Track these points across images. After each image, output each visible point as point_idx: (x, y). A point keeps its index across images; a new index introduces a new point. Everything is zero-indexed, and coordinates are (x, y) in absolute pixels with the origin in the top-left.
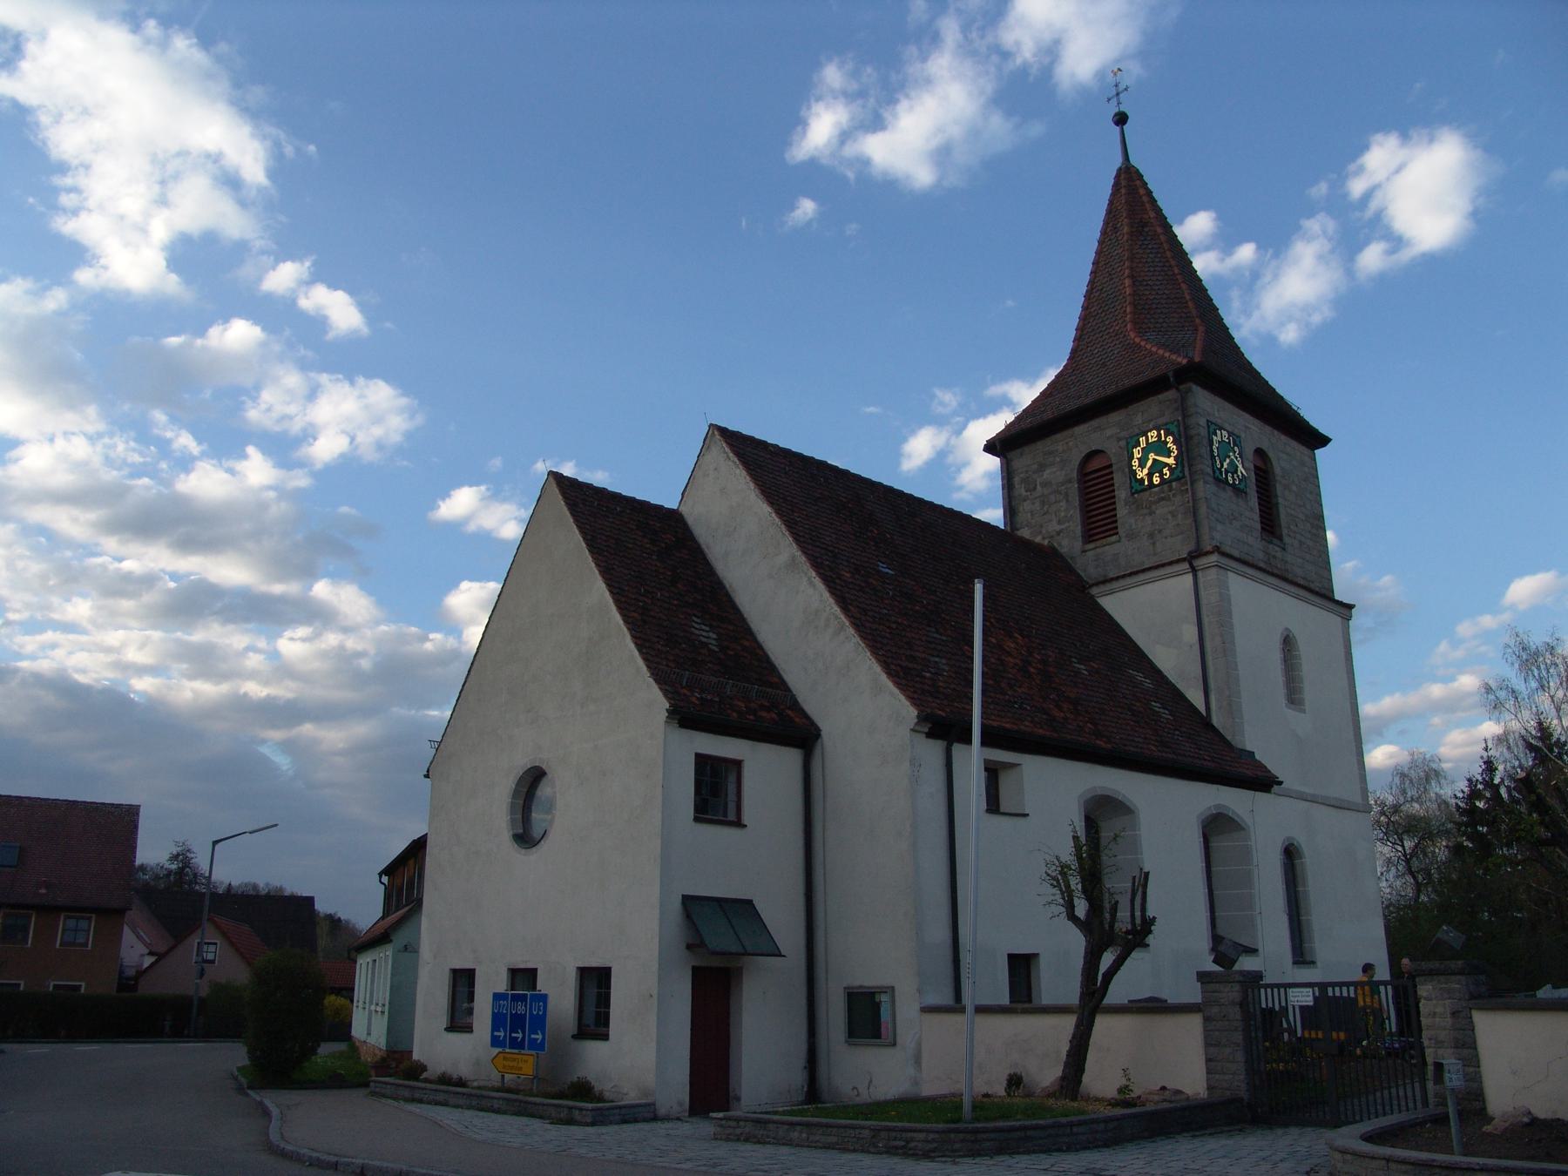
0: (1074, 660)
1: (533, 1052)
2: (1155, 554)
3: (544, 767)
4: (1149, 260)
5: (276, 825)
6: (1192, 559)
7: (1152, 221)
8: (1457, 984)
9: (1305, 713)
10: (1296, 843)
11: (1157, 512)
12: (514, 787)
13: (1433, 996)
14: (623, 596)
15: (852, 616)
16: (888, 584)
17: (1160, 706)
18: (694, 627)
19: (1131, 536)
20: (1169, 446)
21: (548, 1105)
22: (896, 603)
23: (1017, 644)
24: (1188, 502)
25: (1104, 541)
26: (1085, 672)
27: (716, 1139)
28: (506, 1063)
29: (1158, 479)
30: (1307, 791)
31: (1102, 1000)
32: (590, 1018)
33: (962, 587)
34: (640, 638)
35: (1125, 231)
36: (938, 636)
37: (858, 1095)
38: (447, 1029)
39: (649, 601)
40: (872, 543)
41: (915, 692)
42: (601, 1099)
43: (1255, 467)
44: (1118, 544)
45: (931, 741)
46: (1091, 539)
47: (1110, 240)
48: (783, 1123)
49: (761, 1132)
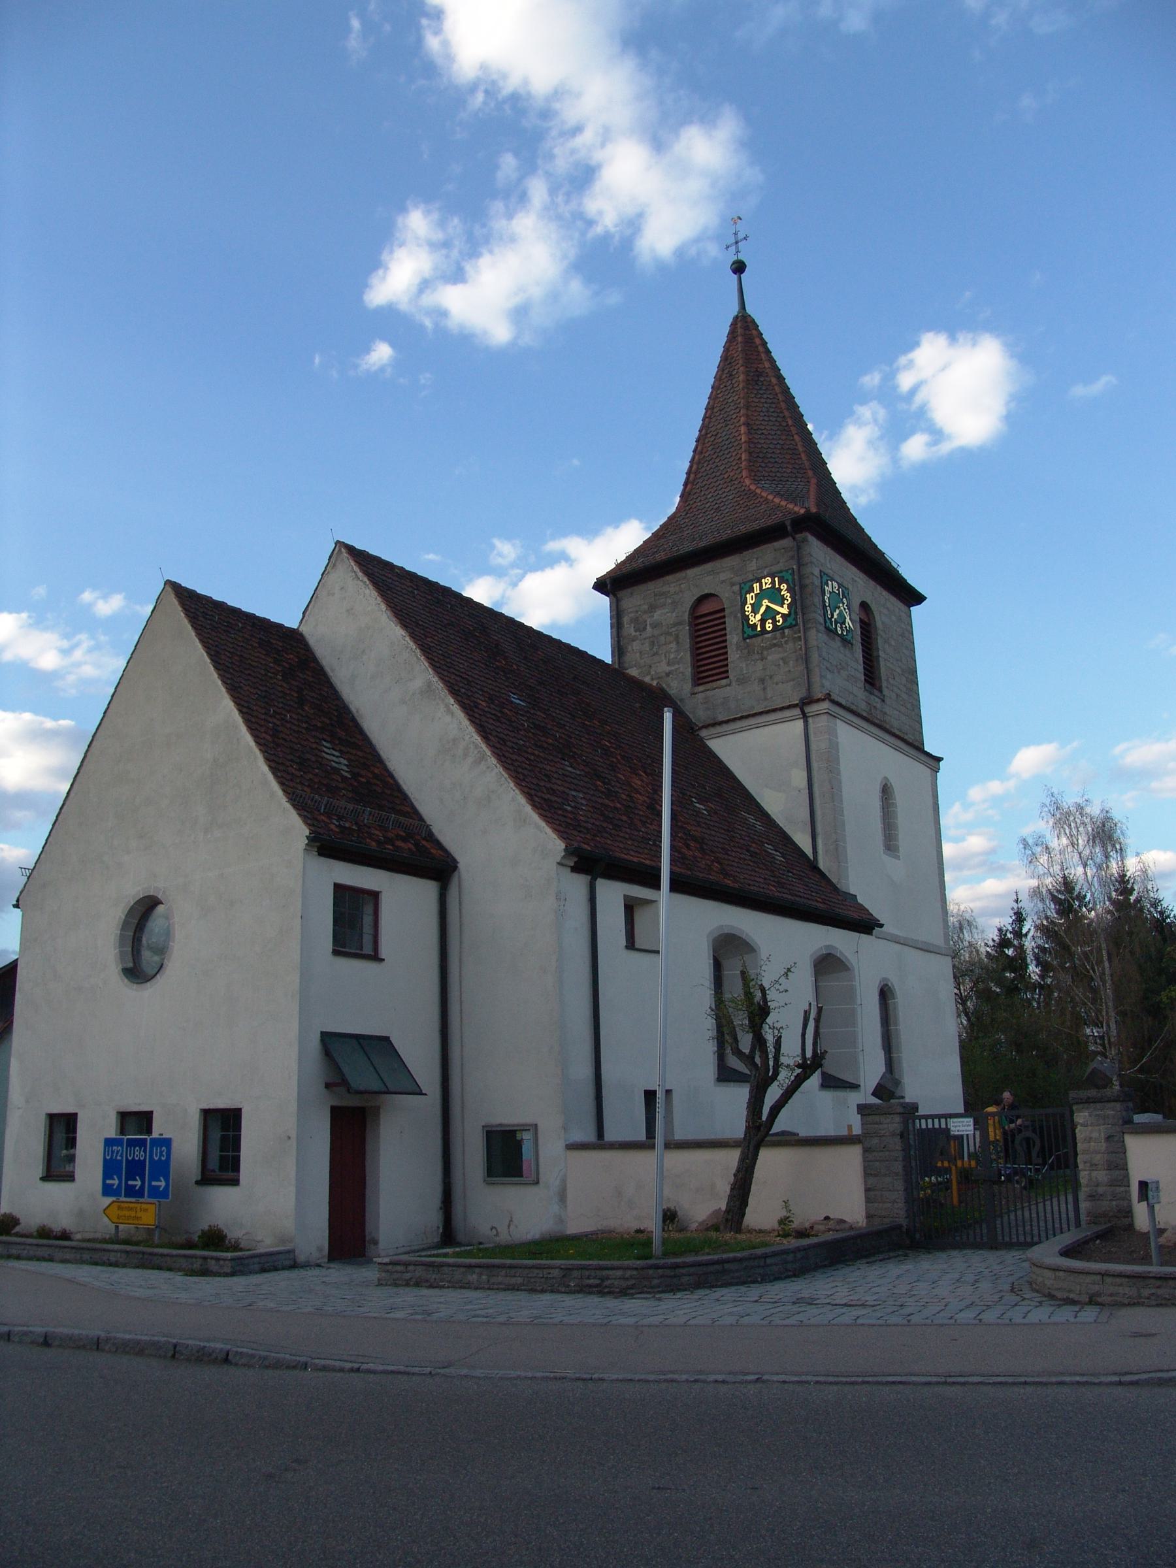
0: (694, 800)
2: (766, 699)
4: (764, 410)
7: (767, 371)
8: (1112, 1111)
11: (769, 658)
12: (124, 917)
15: (494, 746)
17: (772, 848)
18: (324, 752)
19: (742, 681)
20: (782, 593)
25: (714, 685)
29: (771, 625)
32: (214, 1163)
36: (573, 771)
37: (497, 1235)
38: (43, 1179)
41: (560, 825)
42: (236, 1247)
44: (728, 687)
45: (575, 875)
48: (459, 1266)
49: (434, 1277)
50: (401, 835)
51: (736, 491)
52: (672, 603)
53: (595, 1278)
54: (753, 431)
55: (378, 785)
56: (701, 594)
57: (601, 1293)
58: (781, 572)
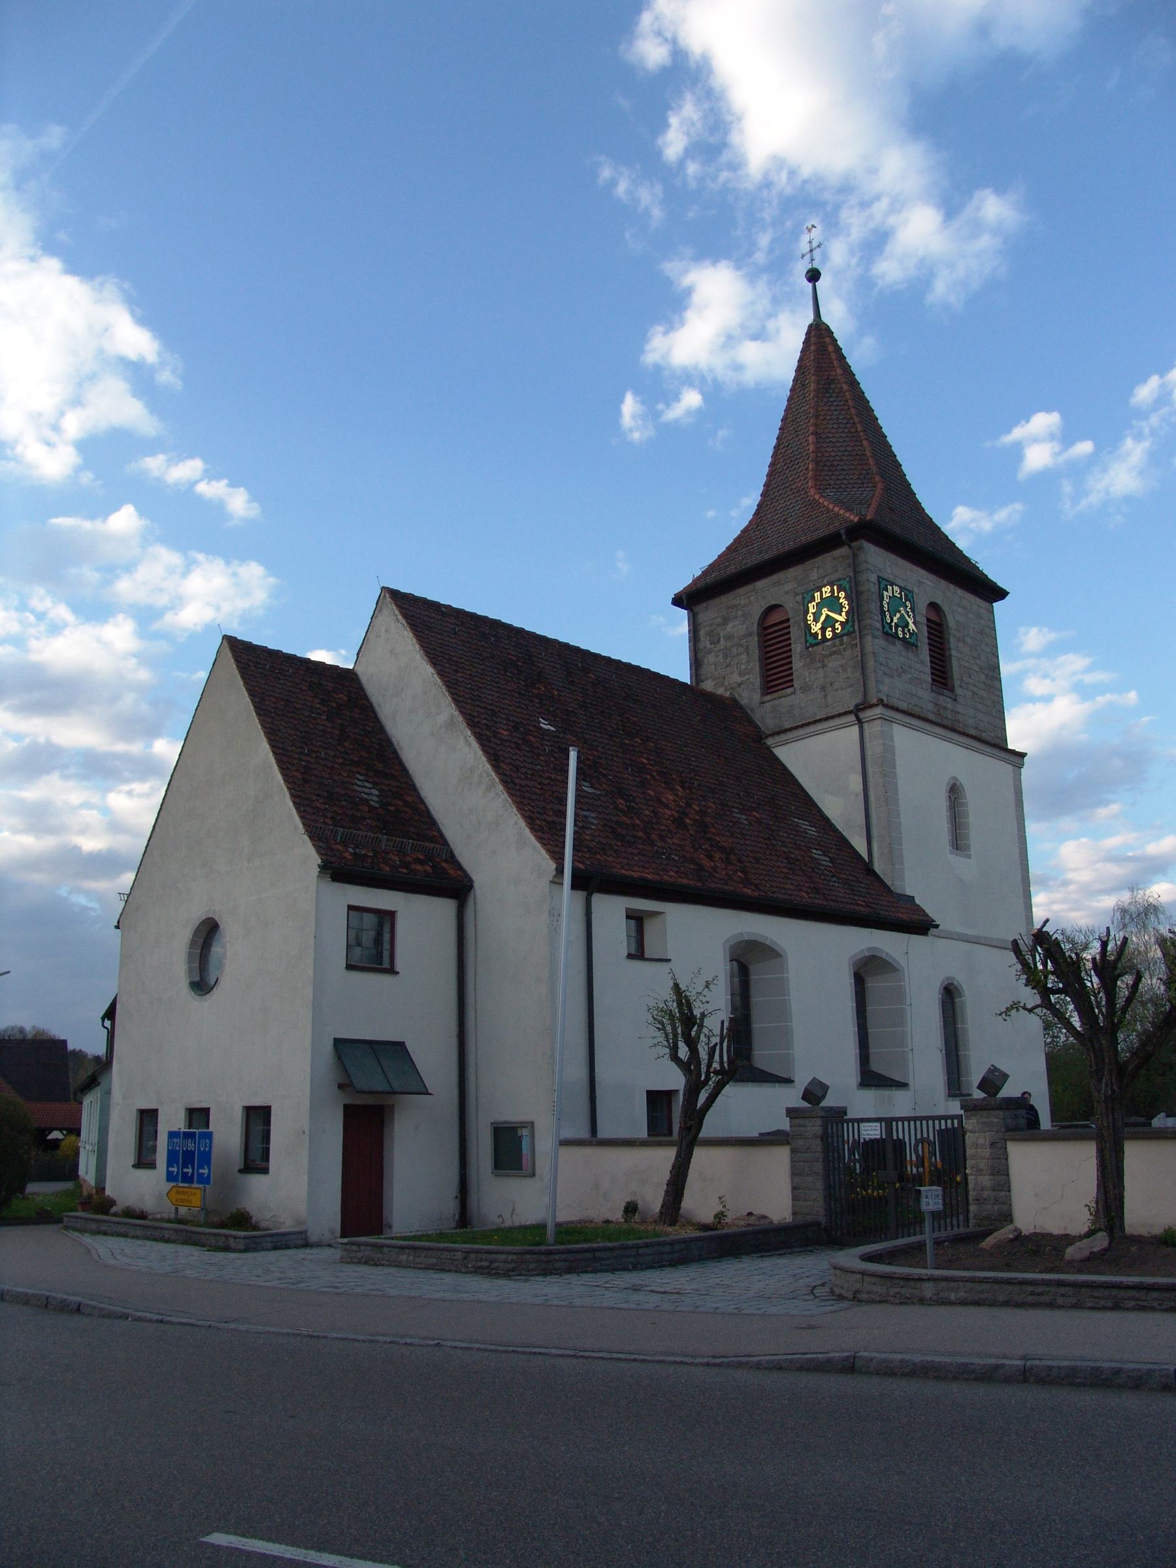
0: (736, 810)
1: (201, 1186)
2: (827, 706)
3: (216, 919)
5: (8, 972)
6: (857, 711)
11: (830, 665)
12: (191, 937)
13: (977, 1129)
16: (547, 740)
17: (820, 853)
19: (806, 688)
20: (841, 601)
23: (677, 795)
25: (779, 694)
26: (746, 822)
27: (342, 1262)
29: (831, 633)
31: (698, 1134)
32: (256, 1154)
33: (627, 741)
34: (299, 797)
35: (812, 387)
37: (503, 1222)
40: (537, 701)
42: (255, 1227)
43: (928, 620)
46: (769, 691)
48: (393, 1247)
50: (419, 859)
53: (486, 1260)
54: (821, 441)
55: (405, 812)
56: (768, 605)
57: (489, 1274)
58: (839, 580)
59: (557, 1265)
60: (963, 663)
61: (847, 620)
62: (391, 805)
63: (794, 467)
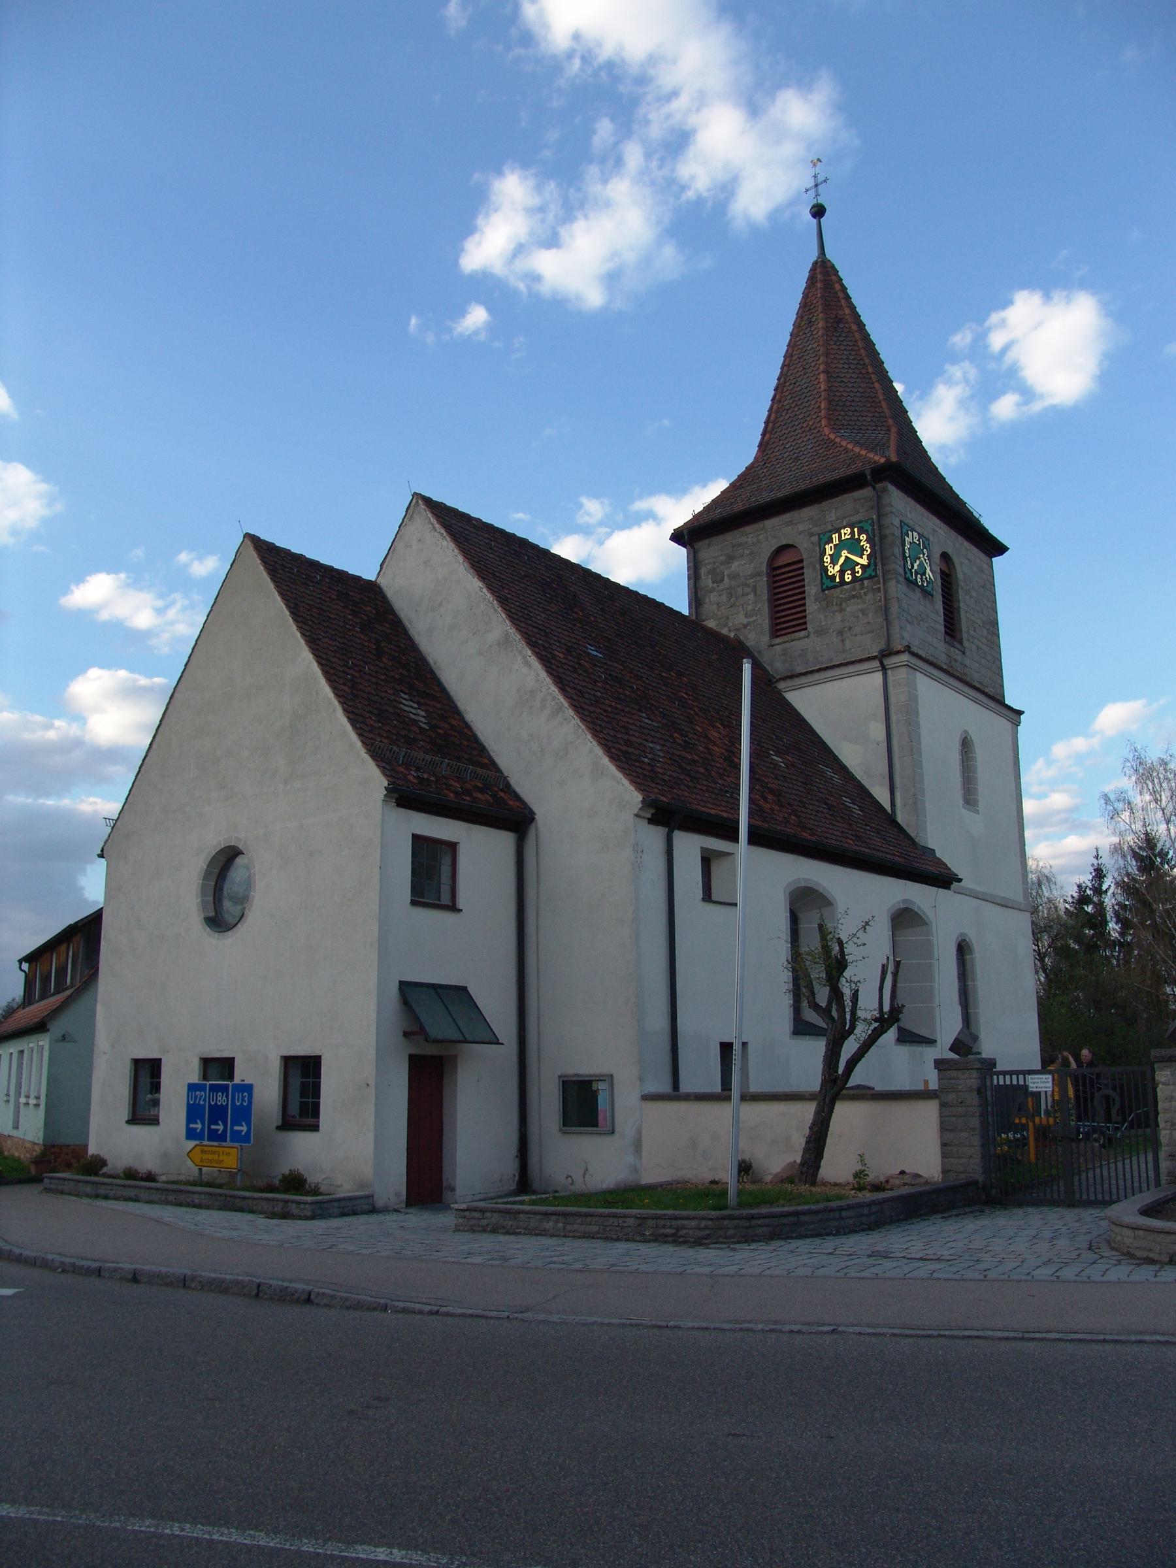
1: (236, 1144)
2: (844, 651)
3: (240, 847)
6: (883, 658)
9: (978, 814)
10: (967, 939)
11: (848, 609)
12: (205, 867)
13: (1171, 1082)
14: (331, 668)
16: (599, 667)
19: (821, 632)
20: (862, 544)
21: (262, 1199)
22: (608, 686)
24: (880, 601)
28: (205, 1156)
30: (978, 889)
32: (294, 1109)
34: (352, 712)
37: (572, 1183)
38: (128, 1122)
39: (357, 675)
42: (316, 1191)
45: (652, 827)
46: (778, 633)
47: (805, 333)
48: (535, 1213)
49: (510, 1223)
51: (815, 440)
52: (750, 554)
53: (670, 1227)
54: (833, 380)
59: (760, 1230)
60: (969, 616)
61: (869, 565)
62: (440, 728)
63: (804, 404)
